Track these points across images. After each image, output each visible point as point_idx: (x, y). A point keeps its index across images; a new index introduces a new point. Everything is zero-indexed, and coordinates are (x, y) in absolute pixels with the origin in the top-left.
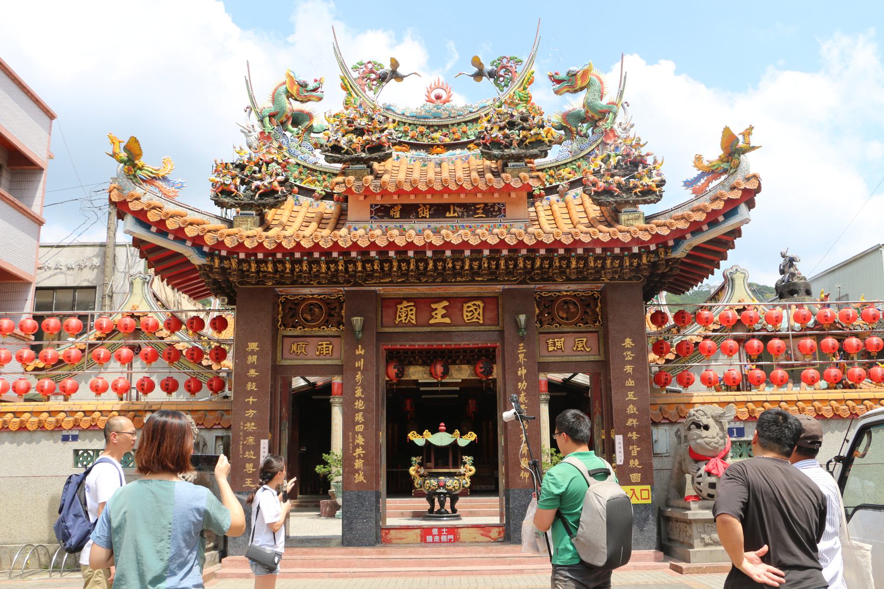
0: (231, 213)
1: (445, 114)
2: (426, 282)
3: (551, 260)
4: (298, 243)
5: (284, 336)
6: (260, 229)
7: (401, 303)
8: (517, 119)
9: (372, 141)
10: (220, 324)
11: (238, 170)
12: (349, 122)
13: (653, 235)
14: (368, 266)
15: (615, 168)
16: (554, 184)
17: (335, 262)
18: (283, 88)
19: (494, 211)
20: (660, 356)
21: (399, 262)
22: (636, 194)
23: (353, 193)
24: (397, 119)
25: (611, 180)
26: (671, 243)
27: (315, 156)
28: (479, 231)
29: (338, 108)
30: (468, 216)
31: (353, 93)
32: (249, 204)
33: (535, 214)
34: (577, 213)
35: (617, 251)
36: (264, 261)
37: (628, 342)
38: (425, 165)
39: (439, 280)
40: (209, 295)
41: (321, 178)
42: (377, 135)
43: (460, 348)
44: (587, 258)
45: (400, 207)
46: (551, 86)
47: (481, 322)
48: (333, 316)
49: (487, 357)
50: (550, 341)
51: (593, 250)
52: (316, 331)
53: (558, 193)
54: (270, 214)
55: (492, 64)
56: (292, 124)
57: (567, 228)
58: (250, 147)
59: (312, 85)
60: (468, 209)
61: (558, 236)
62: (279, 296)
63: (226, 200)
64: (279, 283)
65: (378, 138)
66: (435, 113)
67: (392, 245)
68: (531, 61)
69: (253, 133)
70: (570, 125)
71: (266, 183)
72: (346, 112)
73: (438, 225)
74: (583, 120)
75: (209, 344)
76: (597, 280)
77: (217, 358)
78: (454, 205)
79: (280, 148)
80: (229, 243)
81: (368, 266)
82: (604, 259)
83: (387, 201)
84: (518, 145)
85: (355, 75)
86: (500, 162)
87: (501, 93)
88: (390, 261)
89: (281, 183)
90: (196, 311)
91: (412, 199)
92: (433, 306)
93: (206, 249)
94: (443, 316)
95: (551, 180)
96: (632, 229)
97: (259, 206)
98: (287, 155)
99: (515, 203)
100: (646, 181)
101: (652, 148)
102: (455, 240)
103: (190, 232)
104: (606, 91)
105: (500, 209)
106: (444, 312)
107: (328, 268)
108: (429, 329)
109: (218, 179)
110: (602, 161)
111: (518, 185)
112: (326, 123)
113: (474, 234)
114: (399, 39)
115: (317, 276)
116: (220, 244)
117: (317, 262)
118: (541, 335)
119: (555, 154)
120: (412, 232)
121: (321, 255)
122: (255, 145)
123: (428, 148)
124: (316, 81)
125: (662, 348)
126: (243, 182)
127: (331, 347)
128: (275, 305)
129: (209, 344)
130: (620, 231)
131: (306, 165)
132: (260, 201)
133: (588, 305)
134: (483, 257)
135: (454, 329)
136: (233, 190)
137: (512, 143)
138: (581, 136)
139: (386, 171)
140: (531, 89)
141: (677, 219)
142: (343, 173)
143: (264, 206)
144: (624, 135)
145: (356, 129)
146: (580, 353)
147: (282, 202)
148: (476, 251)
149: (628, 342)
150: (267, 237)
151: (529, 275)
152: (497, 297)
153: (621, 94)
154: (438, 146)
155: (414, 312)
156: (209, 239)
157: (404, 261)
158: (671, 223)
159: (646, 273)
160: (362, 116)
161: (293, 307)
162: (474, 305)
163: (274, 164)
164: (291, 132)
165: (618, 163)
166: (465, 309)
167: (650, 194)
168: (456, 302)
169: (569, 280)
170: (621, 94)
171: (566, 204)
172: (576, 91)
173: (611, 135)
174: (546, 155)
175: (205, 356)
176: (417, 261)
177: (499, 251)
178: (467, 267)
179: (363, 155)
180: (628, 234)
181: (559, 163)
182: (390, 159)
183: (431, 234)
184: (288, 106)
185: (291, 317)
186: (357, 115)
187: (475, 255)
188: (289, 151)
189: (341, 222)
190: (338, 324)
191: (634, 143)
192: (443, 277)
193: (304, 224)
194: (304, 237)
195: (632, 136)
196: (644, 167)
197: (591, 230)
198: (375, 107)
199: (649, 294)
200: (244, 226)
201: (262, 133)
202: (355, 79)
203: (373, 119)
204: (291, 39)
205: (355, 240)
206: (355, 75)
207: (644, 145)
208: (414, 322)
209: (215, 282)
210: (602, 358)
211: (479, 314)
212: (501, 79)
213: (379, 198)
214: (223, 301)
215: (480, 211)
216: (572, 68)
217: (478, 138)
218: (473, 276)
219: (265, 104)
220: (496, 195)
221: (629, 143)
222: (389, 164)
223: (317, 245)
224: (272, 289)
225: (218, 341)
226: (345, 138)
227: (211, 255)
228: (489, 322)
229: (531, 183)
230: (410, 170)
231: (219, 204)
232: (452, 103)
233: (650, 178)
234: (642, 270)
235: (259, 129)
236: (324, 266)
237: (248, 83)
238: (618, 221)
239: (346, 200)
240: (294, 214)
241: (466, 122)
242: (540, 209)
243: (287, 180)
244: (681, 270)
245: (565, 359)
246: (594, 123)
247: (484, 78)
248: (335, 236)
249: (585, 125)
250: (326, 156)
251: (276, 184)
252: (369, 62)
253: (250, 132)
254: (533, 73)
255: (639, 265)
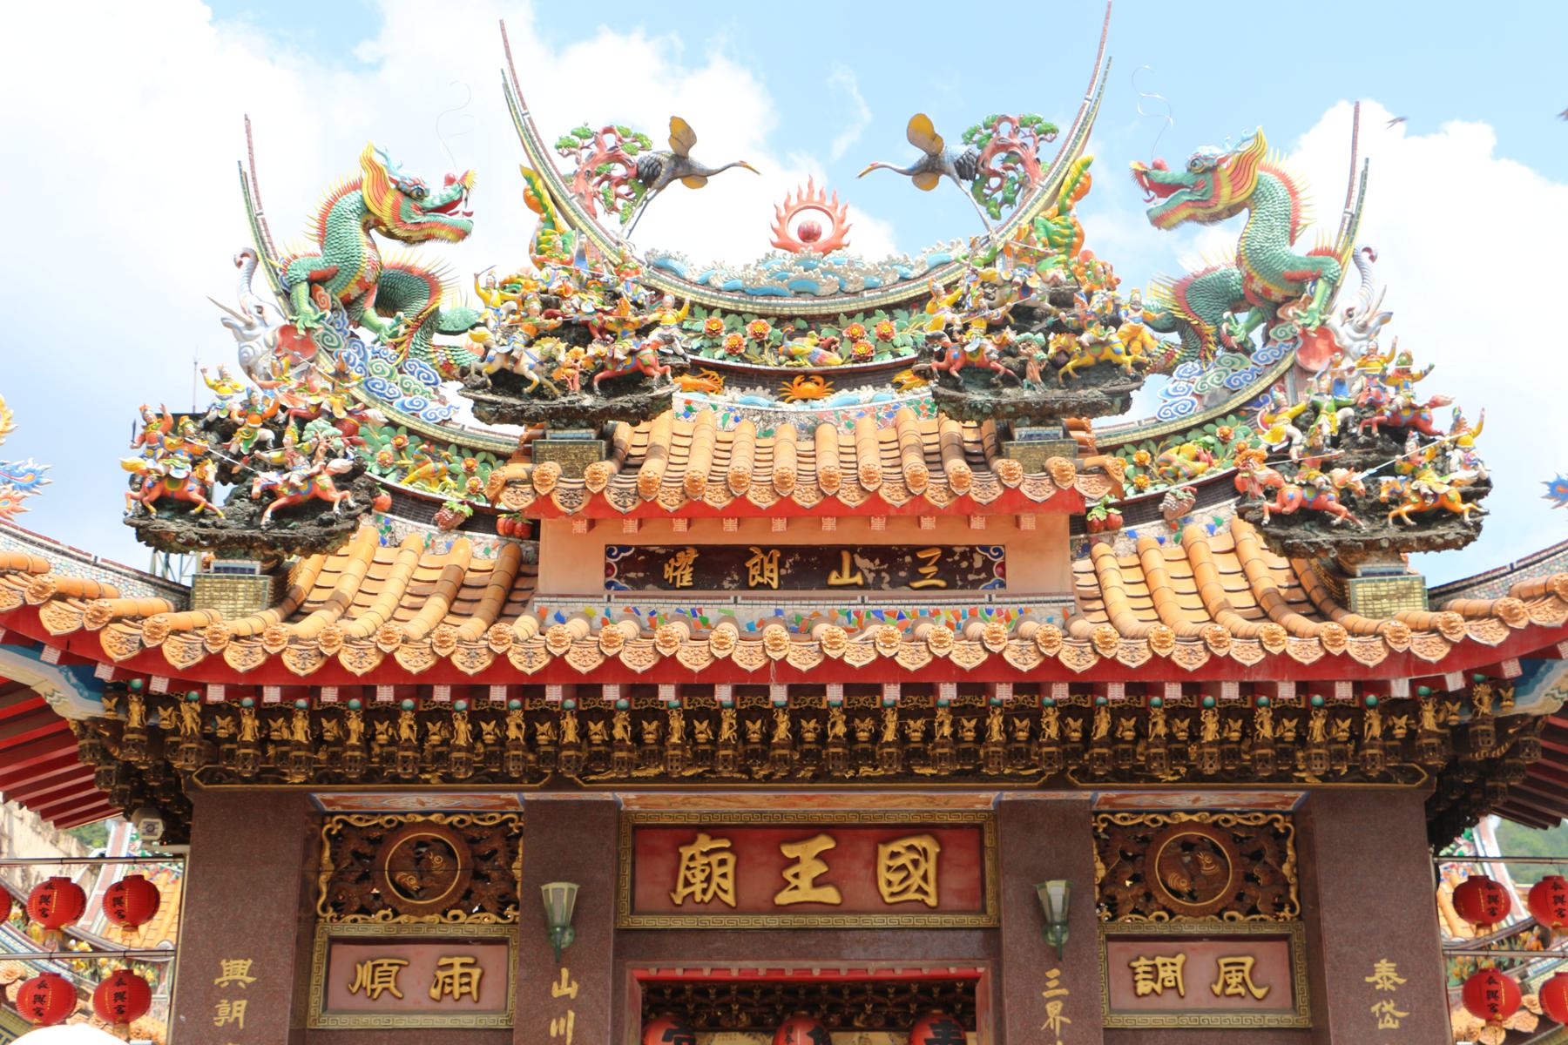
0: (184, 568)
1: (827, 285)
2: (768, 778)
3: (1143, 717)
4: (389, 660)
5: (334, 940)
6: (273, 615)
7: (691, 841)
8: (1039, 298)
9: (614, 360)
10: (135, 901)
11: (213, 437)
12: (546, 304)
13: (1454, 646)
14: (596, 728)
15: (1335, 443)
16: (1150, 491)
17: (498, 715)
18: (354, 197)
19: (970, 569)
20: (1489, 1021)
21: (689, 716)
22: (1398, 520)
23: (554, 512)
24: (688, 298)
25: (1321, 479)
26: (1512, 669)
27: (443, 401)
28: (925, 629)
29: (515, 261)
30: (894, 584)
31: (560, 220)
32: (242, 541)
33: (1092, 579)
34: (1220, 578)
35: (1343, 691)
36: (284, 712)
37: (1385, 973)
38: (767, 434)
39: (806, 773)
40: (104, 811)
41: (459, 466)
42: (630, 343)
43: (865, 982)
44: (1252, 712)
45: (693, 555)
46: (1142, 203)
47: (932, 901)
48: (487, 878)
49: (948, 1007)
50: (1142, 965)
51: (1270, 689)
52: (433, 924)
53: (1161, 516)
54: (305, 571)
55: (968, 138)
56: (377, 306)
57: (1189, 620)
58: (249, 371)
59: (437, 194)
60: (895, 564)
61: (1163, 644)
62: (323, 816)
63: (172, 527)
64: (326, 778)
65: (632, 353)
66: (801, 278)
67: (667, 666)
68: (1084, 129)
69: (259, 330)
70: (1196, 318)
71: (295, 478)
72: (538, 274)
73: (805, 610)
74: (1237, 303)
75: (92, 962)
76: (1283, 778)
77: (120, 1011)
78: (852, 549)
79: (341, 375)
80: (178, 655)
81: (596, 728)
82: (1304, 716)
83: (655, 537)
84: (1045, 375)
85: (567, 166)
86: (990, 426)
87: (993, 224)
88: (660, 714)
89: (342, 480)
90: (61, 861)
91: (730, 533)
92: (789, 851)
93: (104, 673)
94: (817, 883)
95: (1141, 479)
96: (1387, 626)
97: (272, 545)
98: (361, 396)
99: (1035, 547)
100: (1430, 481)
101: (1449, 384)
102: (857, 656)
103: (57, 620)
104: (1305, 215)
105: (987, 565)
106: (820, 868)
107: (477, 735)
108: (774, 922)
109: (149, 464)
110: (1295, 422)
111: (1044, 493)
112: (477, 305)
113: (912, 637)
114: (694, 60)
115: (440, 758)
116: (151, 658)
117: (443, 715)
118: (1113, 946)
119: (1152, 402)
120: (729, 630)
121: (456, 695)
122: (265, 362)
123: (777, 381)
124: (450, 181)
125: (1495, 994)
126: (225, 475)
127: (476, 973)
128: (311, 845)
129: (92, 962)
130: (1353, 633)
131: (416, 426)
132: (276, 532)
133: (1257, 856)
134: (937, 706)
135: (848, 921)
136: (195, 496)
137: (1023, 370)
138: (1231, 350)
139: (653, 450)
140: (1078, 210)
141: (1529, 597)
142: (528, 452)
143: (289, 545)
144: (1361, 347)
145: (567, 324)
146: (1235, 1003)
147: (344, 536)
148: (919, 686)
149: (1385, 973)
150: (294, 639)
151: (1074, 763)
152: (979, 828)
153: (1351, 224)
154: (807, 376)
155: (729, 869)
156: (116, 645)
157: (702, 713)
158: (1510, 610)
159: (1435, 761)
160: (584, 287)
161: (368, 850)
162: (911, 848)
163: (321, 422)
164: (374, 330)
165: (1344, 428)
166: (884, 861)
167: (1440, 522)
168: (857, 839)
169: (1196, 778)
170: (1351, 224)
171: (1187, 549)
172: (1215, 218)
173: (1321, 345)
174: (1126, 405)
175: (80, 1003)
176: (742, 716)
177: (986, 690)
178: (889, 736)
179: (588, 400)
180: (1378, 642)
181: (1164, 430)
182: (666, 415)
183: (785, 634)
184: (368, 251)
185: (359, 880)
186: (572, 285)
187: (913, 700)
188: (367, 386)
189: (517, 597)
190: (503, 902)
191: (1391, 368)
192: (818, 763)
193: (407, 601)
194: (406, 641)
195: (1384, 349)
196: (1422, 442)
197: (1262, 628)
198: (625, 260)
199: (1446, 824)
200: (224, 606)
201: (285, 330)
202: (566, 179)
203: (617, 296)
204: (365, 51)
205: (557, 652)
206: (567, 166)
207: (1425, 374)
208: (729, 899)
209: (128, 771)
210: (1303, 1021)
211: (925, 878)
212: (995, 182)
213: (631, 526)
214: (150, 830)
215: (930, 569)
216: (1205, 151)
217: (925, 354)
218: (908, 762)
219: (298, 244)
220: (978, 523)
221: (1375, 368)
222: (661, 428)
223: (444, 664)
224: (303, 796)
225: (127, 957)
226: (535, 351)
227: (118, 690)
228: (954, 902)
229: (1080, 488)
230: (724, 448)
231: (144, 535)
232: (851, 252)
233: (1442, 472)
234: (1421, 751)
235: (276, 318)
236: (462, 727)
237: (248, 182)
238: (1343, 602)
239: (533, 531)
240: (375, 571)
241: (889, 309)
242: (1107, 563)
243: (358, 470)
244: (1546, 753)
245: (1187, 1021)
246: (1271, 311)
247: (943, 178)
248: (499, 640)
249: (1243, 317)
250: (478, 402)
251: (325, 481)
252: (608, 130)
253: (249, 326)
254: (1087, 164)
255: (1411, 734)
